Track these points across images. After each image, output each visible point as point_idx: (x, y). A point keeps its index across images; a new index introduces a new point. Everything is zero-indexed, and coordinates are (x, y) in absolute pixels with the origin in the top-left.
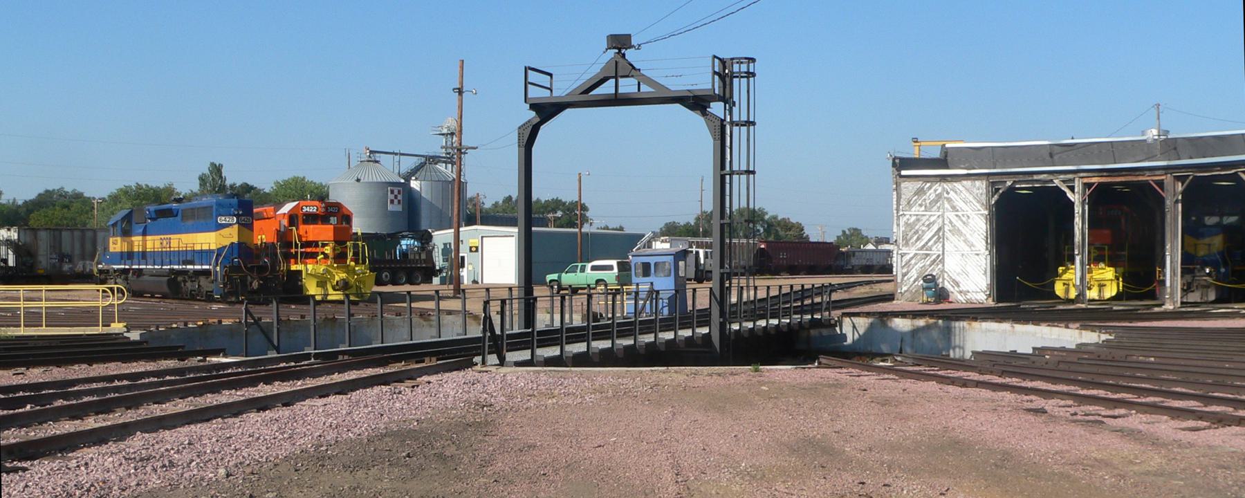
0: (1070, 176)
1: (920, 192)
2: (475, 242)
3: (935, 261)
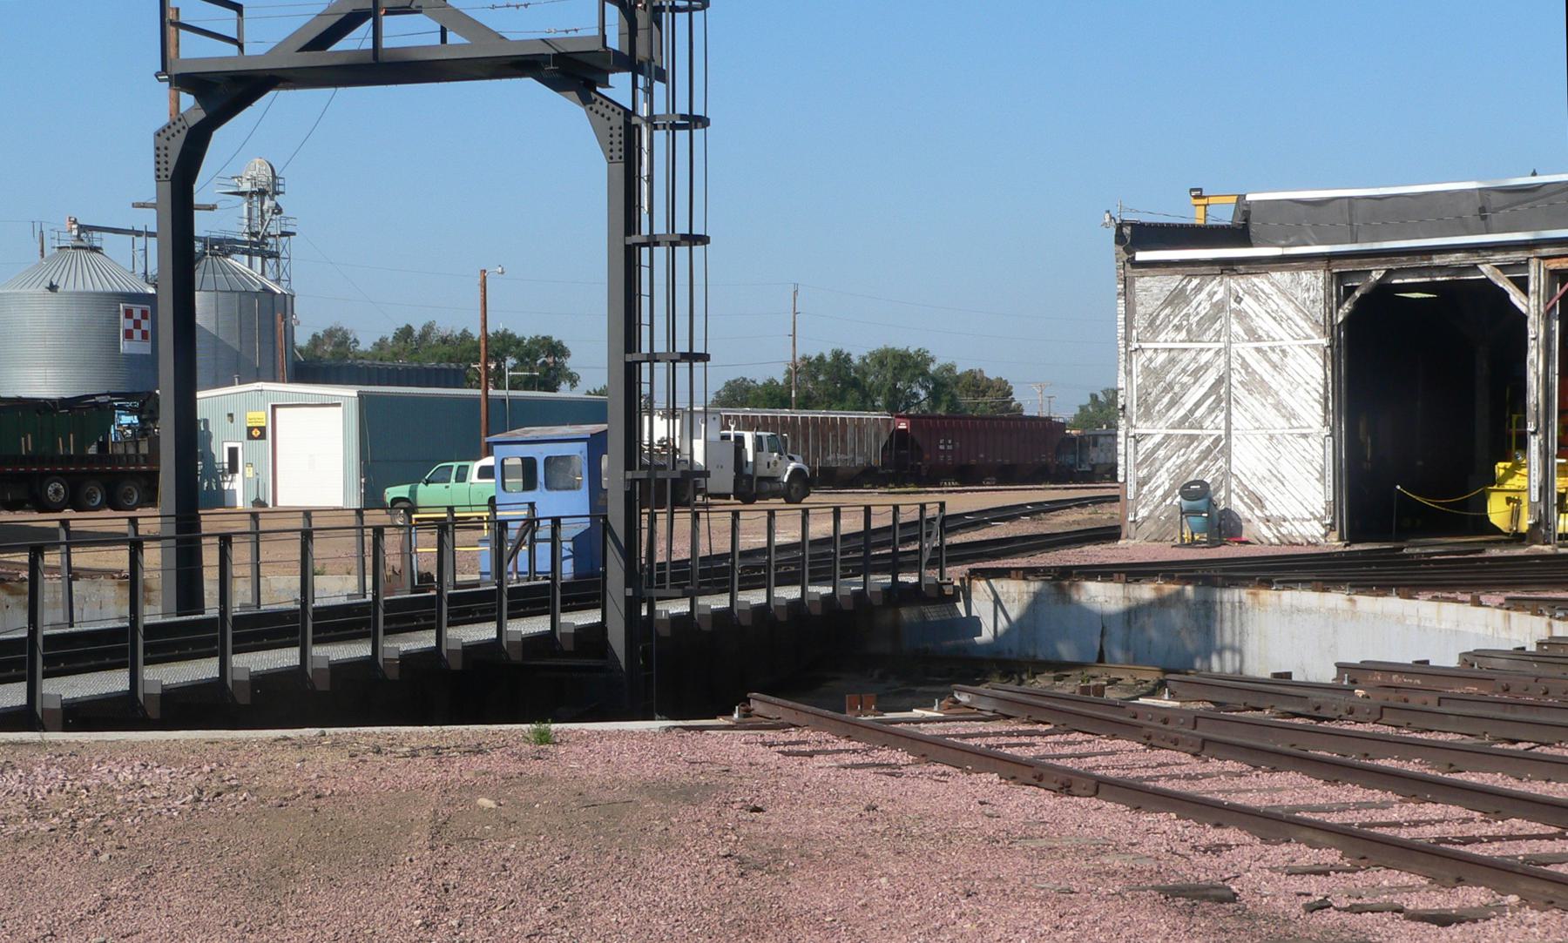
1: (1176, 299)
2: (260, 417)
3: (1209, 451)
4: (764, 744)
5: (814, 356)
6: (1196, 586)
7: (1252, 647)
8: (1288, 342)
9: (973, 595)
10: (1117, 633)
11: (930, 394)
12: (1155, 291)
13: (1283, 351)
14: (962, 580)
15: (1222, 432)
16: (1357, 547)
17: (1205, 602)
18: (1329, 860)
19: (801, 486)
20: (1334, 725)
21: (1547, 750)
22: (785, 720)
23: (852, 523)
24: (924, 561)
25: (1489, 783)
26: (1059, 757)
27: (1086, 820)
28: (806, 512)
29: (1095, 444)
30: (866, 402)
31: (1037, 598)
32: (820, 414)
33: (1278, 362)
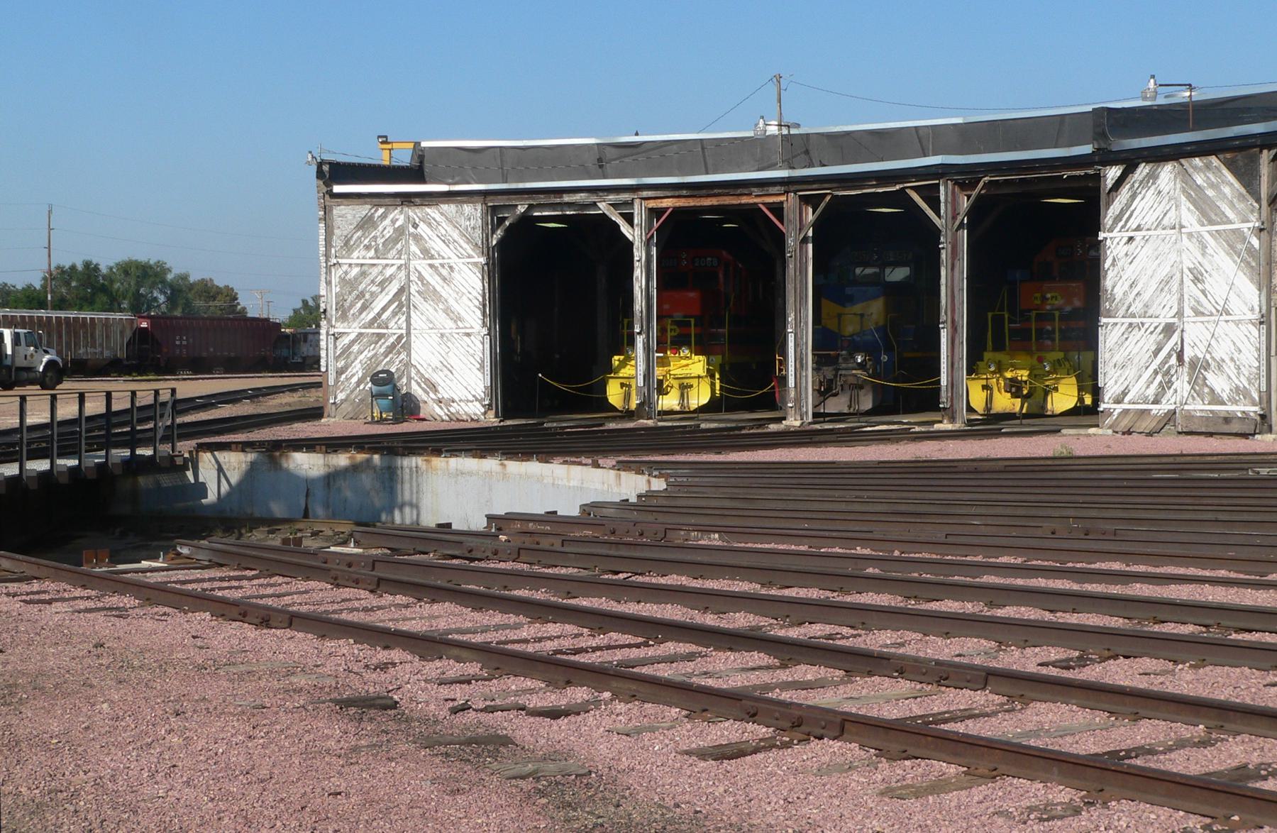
0: (625, 197)
1: (366, 224)
3: (393, 346)
4: (8, 595)
5: (67, 265)
6: (382, 455)
7: (426, 503)
8: (454, 260)
9: (200, 465)
10: (319, 493)
11: (168, 299)
12: (350, 217)
13: (451, 267)
14: (190, 452)
15: (404, 332)
16: (509, 423)
17: (389, 468)
18: (471, 671)
19: (52, 377)
20: (482, 564)
21: (640, 579)
22: (29, 573)
23: (95, 407)
24: (159, 437)
25: (596, 606)
26: (262, 597)
27: (280, 647)
28: (54, 398)
29: (305, 341)
30: (113, 305)
31: (253, 464)
32: (72, 314)
33: (447, 276)
